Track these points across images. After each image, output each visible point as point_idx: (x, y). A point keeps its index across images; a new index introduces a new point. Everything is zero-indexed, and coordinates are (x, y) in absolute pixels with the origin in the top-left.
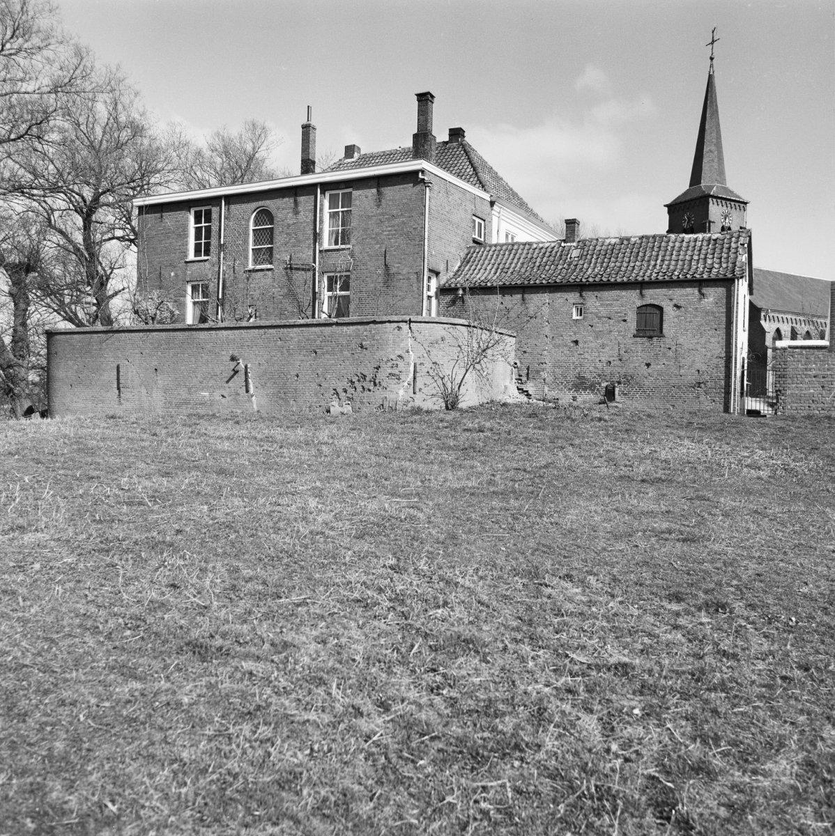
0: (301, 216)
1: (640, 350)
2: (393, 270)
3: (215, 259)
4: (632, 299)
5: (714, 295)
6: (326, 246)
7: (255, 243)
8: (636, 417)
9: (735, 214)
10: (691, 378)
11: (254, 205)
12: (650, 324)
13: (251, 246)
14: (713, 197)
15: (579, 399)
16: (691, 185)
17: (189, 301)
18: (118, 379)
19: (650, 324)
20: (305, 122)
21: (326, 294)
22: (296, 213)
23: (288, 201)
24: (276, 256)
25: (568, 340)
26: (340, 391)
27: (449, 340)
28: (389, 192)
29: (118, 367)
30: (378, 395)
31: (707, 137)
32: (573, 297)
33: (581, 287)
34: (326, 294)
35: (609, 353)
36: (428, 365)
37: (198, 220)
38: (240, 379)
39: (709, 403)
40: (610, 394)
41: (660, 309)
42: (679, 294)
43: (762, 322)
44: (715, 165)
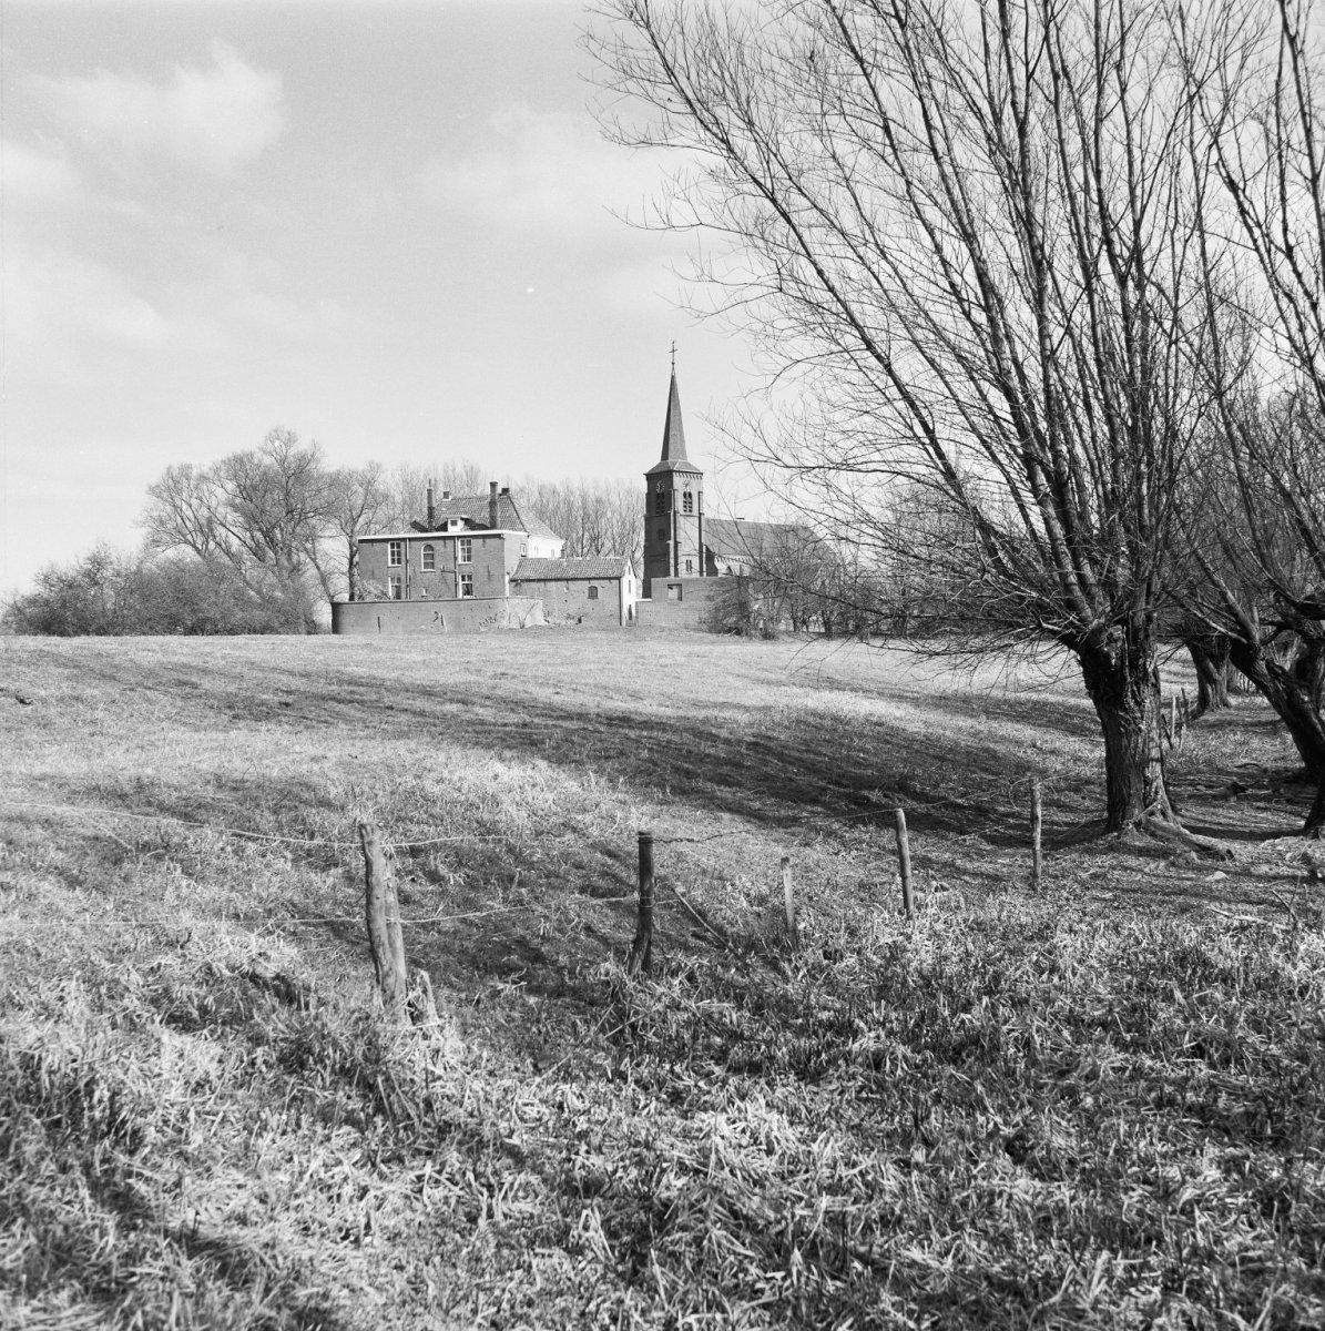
4: (586, 584)
5: (615, 582)
9: (694, 482)
12: (593, 593)
19: (593, 593)
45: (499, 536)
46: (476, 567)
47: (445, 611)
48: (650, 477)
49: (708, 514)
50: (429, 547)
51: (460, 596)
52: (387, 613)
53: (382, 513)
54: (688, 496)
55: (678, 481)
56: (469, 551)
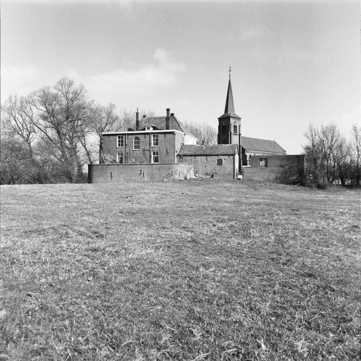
0: (147, 139)
1: (218, 168)
2: (168, 152)
3: (125, 147)
4: (216, 158)
5: (231, 157)
6: (152, 146)
7: (135, 144)
8: (218, 180)
9: (238, 122)
10: (228, 173)
11: (134, 136)
12: (220, 162)
13: (134, 145)
14: (231, 117)
15: (207, 177)
16: (225, 113)
17: (117, 157)
18: (111, 175)
19: (220, 162)
20: (136, 112)
21: (153, 156)
22: (145, 138)
23: (143, 136)
24: (140, 147)
25: (204, 166)
26: (165, 177)
27: (185, 167)
28: (167, 135)
29: (111, 173)
30: (172, 177)
31: (229, 99)
32: (205, 157)
33: (206, 155)
34: (153, 156)
35: (212, 168)
36: (181, 172)
37: (119, 138)
38: (142, 175)
39: (231, 178)
40: (212, 176)
41: (222, 160)
42: (225, 157)
43: (246, 153)
44: (232, 107)
45: (173, 133)
46: (161, 148)
47: (146, 170)
48: (220, 119)
49: (243, 135)
50: (137, 138)
51: (152, 162)
52: (115, 171)
53: (115, 125)
54: (235, 127)
55: (232, 121)
56: (157, 140)
